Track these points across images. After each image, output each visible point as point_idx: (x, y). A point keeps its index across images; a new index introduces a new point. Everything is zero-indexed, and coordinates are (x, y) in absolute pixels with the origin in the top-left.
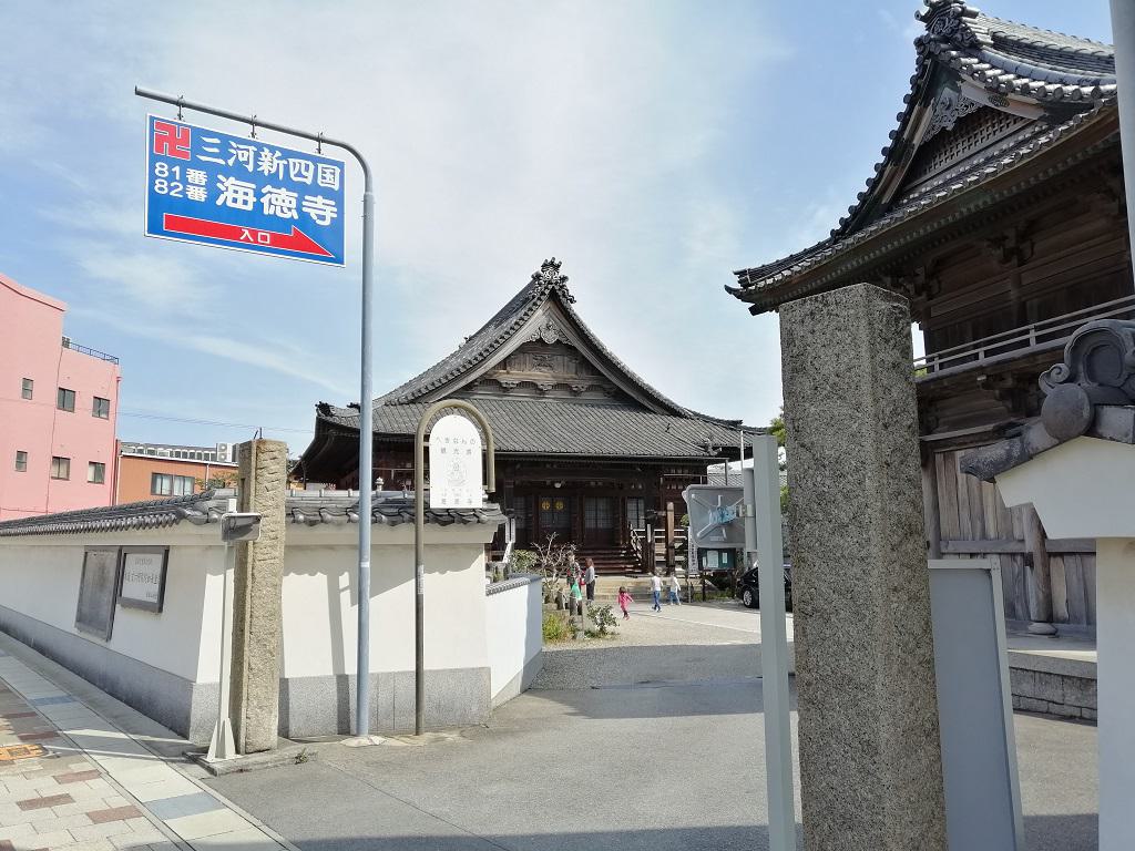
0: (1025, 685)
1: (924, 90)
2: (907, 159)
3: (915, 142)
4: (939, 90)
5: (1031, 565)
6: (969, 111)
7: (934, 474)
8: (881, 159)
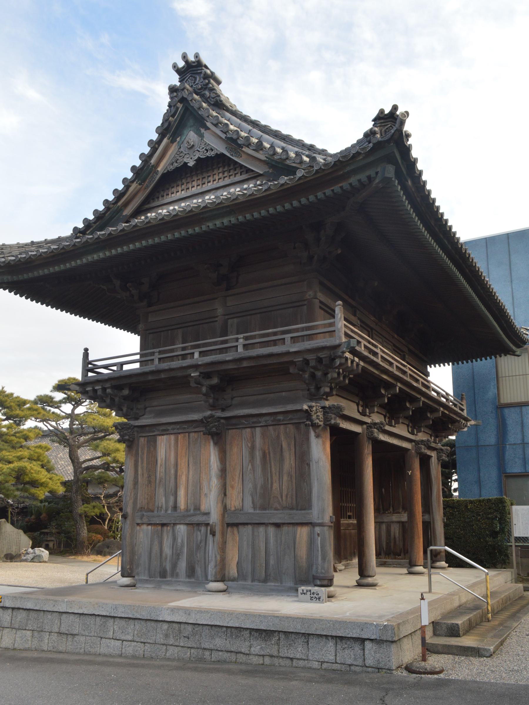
0: (217, 639)
1: (170, 129)
2: (150, 180)
3: (159, 169)
4: (185, 132)
5: (213, 534)
6: (208, 154)
7: (137, 454)
8: (130, 175)
